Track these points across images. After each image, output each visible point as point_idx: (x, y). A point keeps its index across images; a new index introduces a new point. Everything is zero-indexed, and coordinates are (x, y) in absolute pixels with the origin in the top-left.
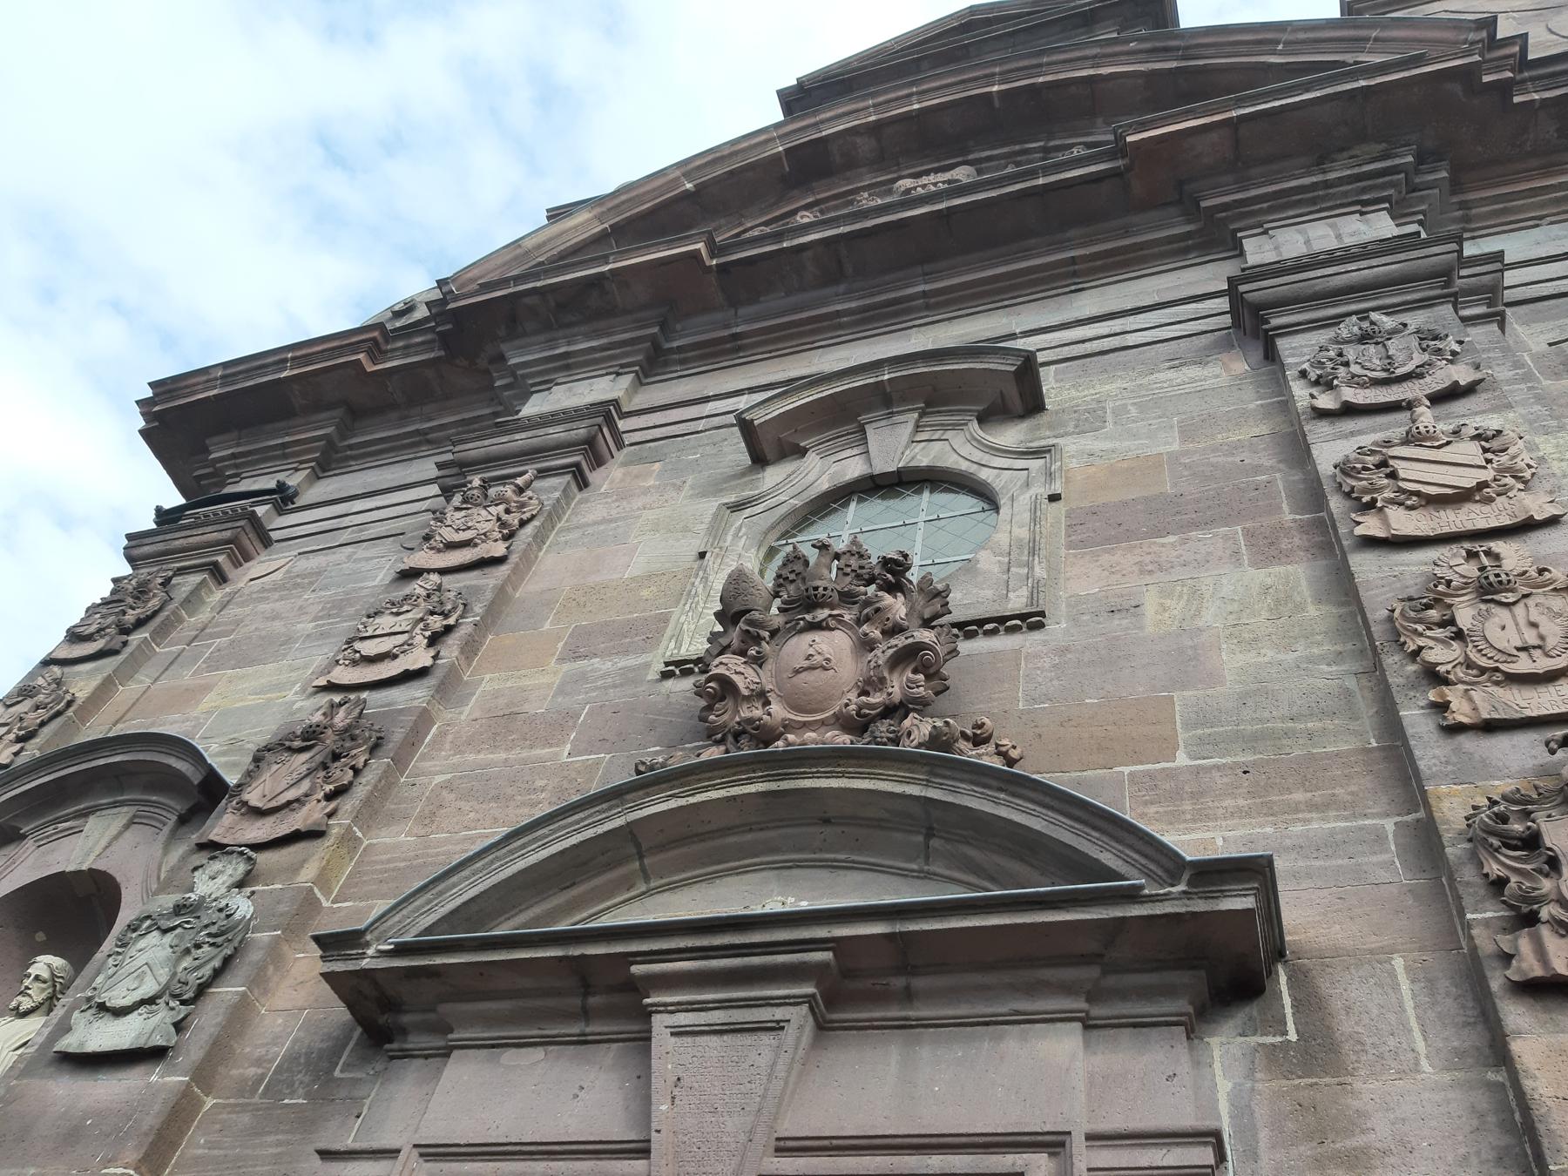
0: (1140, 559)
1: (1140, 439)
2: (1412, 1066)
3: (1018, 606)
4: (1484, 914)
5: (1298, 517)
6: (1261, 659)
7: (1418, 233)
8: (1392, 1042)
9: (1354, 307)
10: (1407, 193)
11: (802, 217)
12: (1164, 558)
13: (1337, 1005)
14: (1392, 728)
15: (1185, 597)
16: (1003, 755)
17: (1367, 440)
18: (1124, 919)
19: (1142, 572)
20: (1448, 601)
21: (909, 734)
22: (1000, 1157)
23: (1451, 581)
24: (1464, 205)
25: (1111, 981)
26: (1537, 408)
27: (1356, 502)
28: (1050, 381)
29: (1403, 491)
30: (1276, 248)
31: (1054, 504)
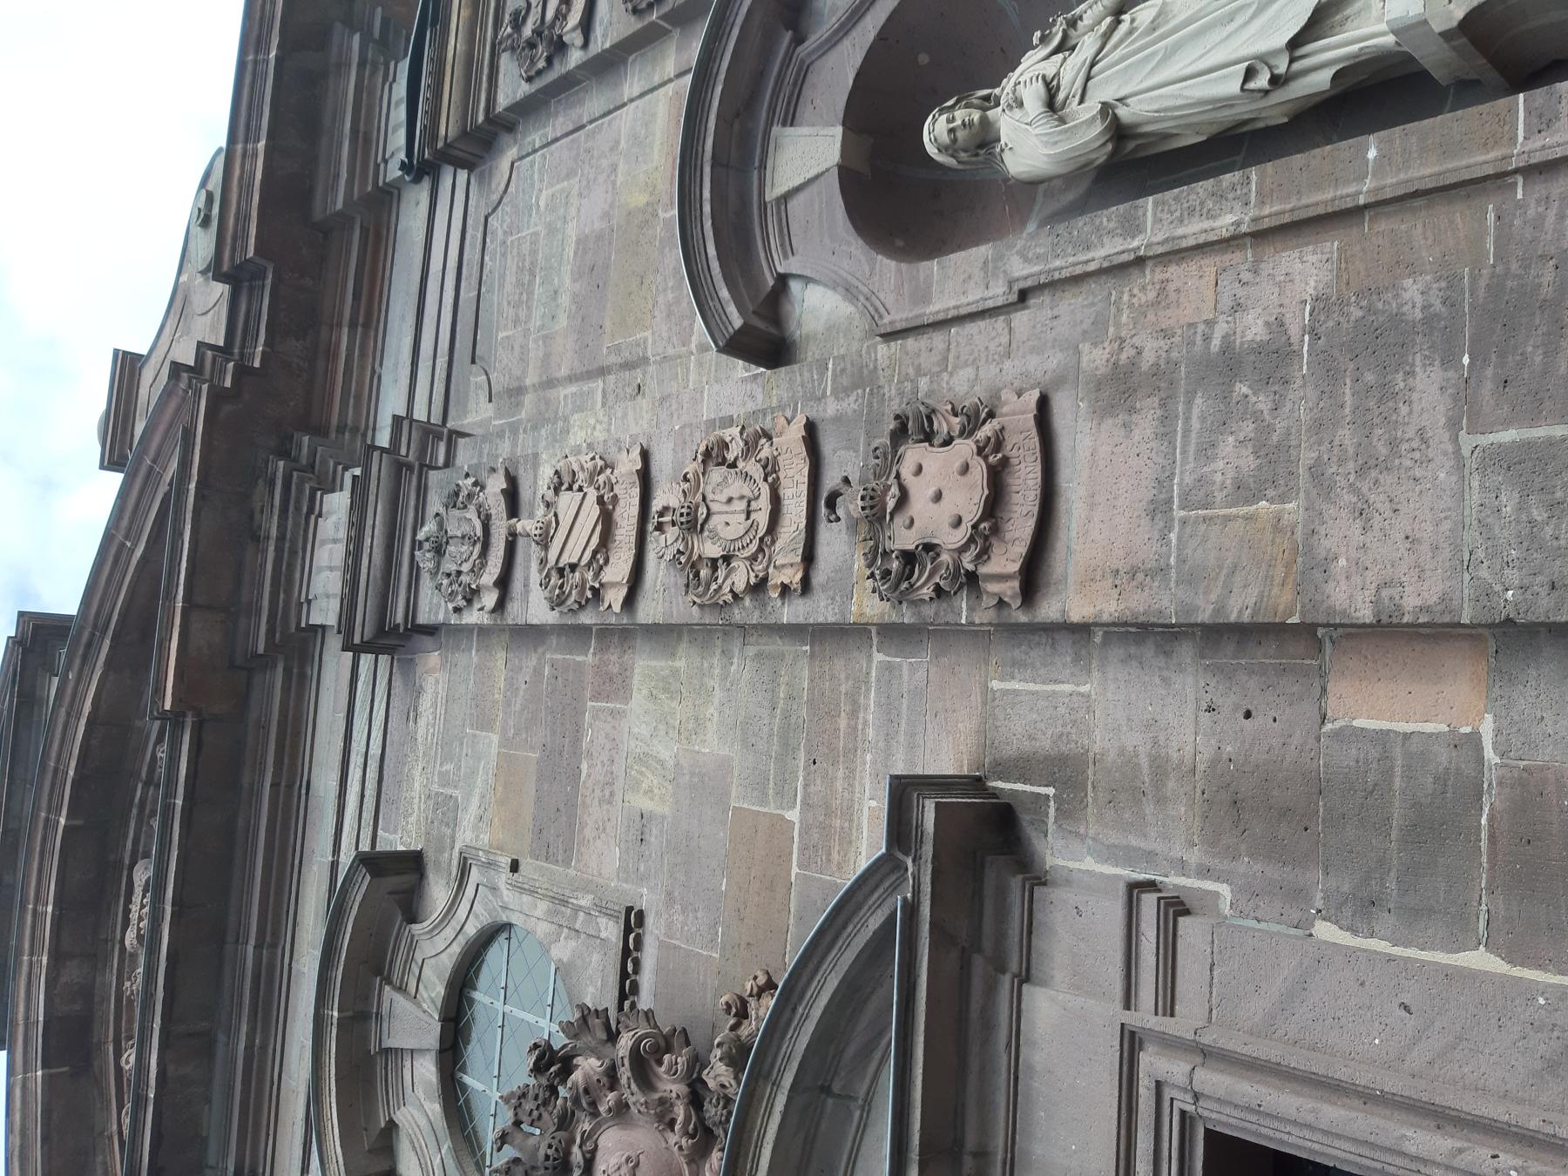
0: (597, 800)
1: (478, 767)
2: (1084, 700)
3: (615, 932)
4: (963, 610)
5: (592, 650)
6: (715, 719)
7: (354, 477)
8: (1062, 710)
9: (407, 549)
10: (314, 473)
11: (127, 1062)
12: (601, 778)
13: (1027, 746)
14: (796, 631)
15: (644, 769)
16: (760, 992)
17: (535, 577)
18: (932, 924)
19: (610, 803)
20: (695, 558)
21: (723, 1086)
22: (1140, 1101)
23: (678, 550)
24: (341, 429)
25: (987, 944)
26: (543, 432)
27: (590, 602)
28: (395, 840)
29: (589, 565)
30: (328, 596)
31: (521, 868)
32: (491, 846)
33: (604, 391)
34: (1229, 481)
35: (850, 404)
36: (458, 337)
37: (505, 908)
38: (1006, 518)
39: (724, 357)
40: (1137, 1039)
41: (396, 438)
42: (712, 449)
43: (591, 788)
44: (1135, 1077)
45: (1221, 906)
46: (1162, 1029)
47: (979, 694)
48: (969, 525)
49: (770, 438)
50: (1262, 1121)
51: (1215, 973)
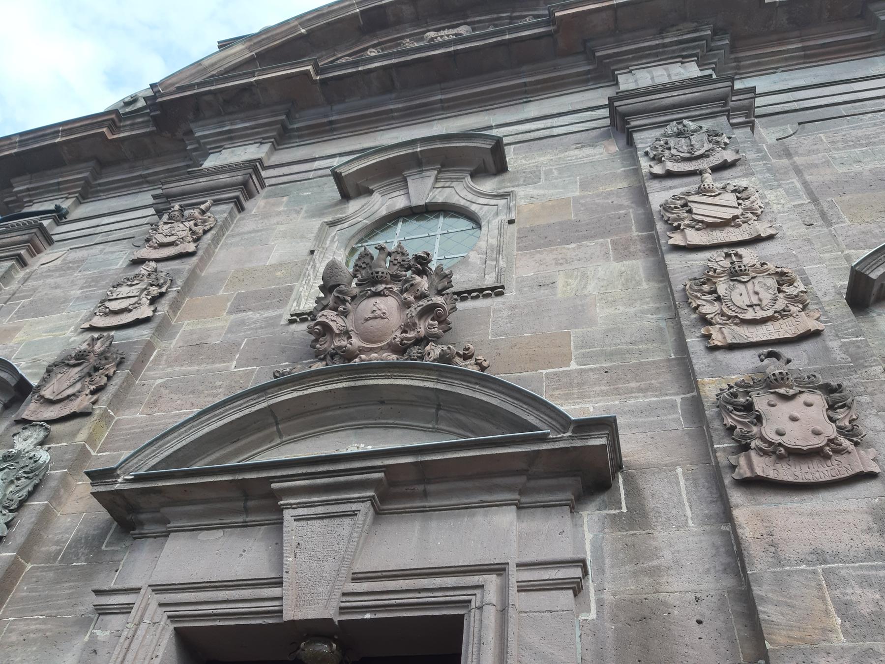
0: (556, 256)
1: (559, 189)
4: (723, 445)
5: (640, 234)
7: (711, 75)
8: (674, 511)
10: (707, 52)
11: (371, 52)
13: (647, 493)
14: (682, 348)
15: (579, 278)
17: (678, 192)
19: (556, 264)
20: (714, 280)
21: (429, 354)
23: (716, 269)
24: (737, 60)
25: (532, 483)
26: (768, 175)
28: (512, 156)
29: (694, 220)
31: (511, 225)
32: (519, 207)
33: (802, 204)
34: (848, 597)
35: (839, 356)
36: (814, 111)
37: (489, 222)
38: (790, 463)
39: (848, 273)
40: (501, 572)
41: (742, 92)
42: (787, 276)
43: (561, 252)
44: (482, 573)
45: (583, 614)
46: (511, 586)
47: (671, 461)
48: (781, 441)
49: (803, 309)
50: (475, 645)
51: (547, 613)
